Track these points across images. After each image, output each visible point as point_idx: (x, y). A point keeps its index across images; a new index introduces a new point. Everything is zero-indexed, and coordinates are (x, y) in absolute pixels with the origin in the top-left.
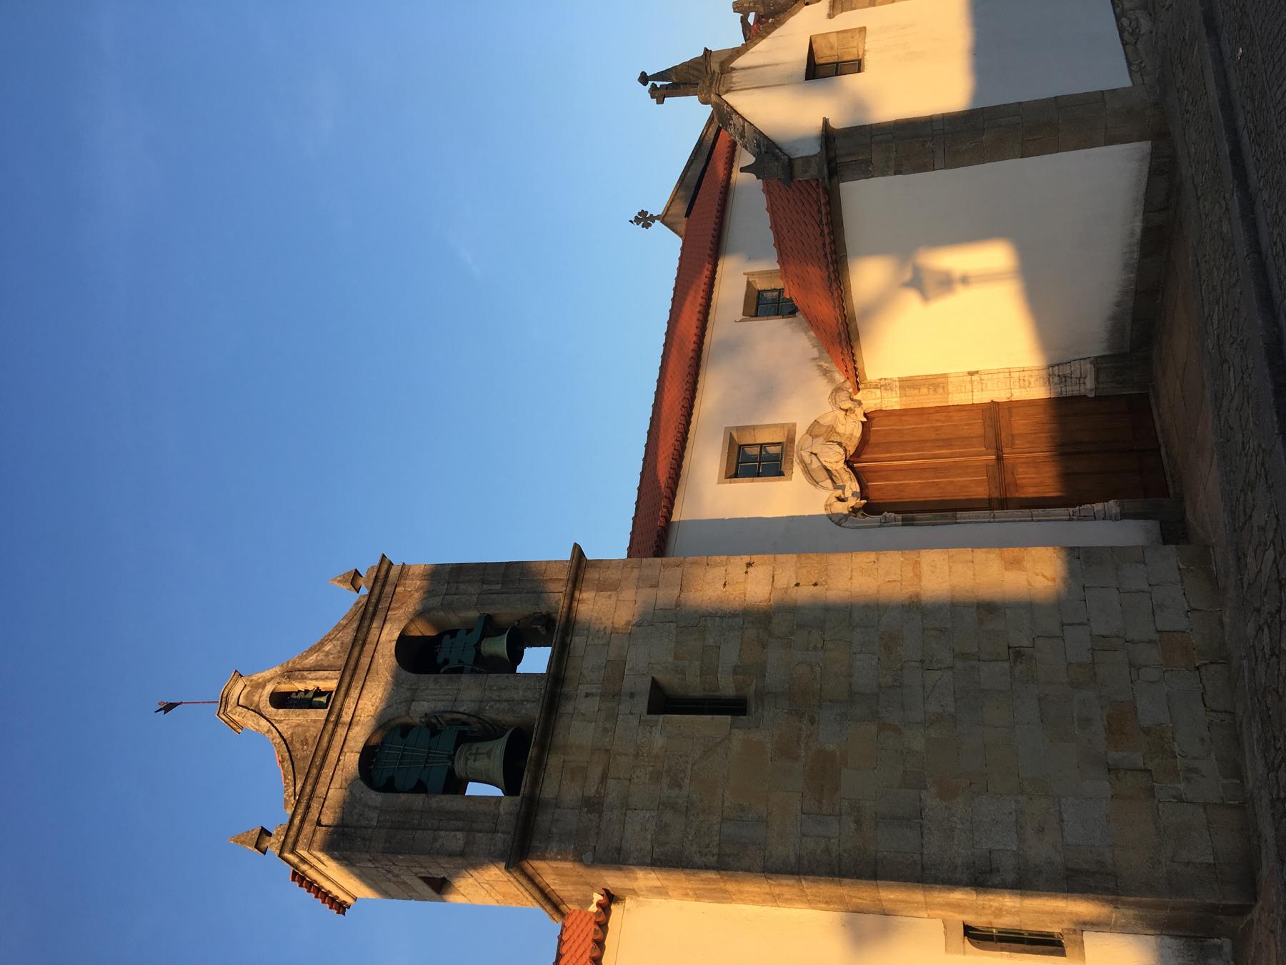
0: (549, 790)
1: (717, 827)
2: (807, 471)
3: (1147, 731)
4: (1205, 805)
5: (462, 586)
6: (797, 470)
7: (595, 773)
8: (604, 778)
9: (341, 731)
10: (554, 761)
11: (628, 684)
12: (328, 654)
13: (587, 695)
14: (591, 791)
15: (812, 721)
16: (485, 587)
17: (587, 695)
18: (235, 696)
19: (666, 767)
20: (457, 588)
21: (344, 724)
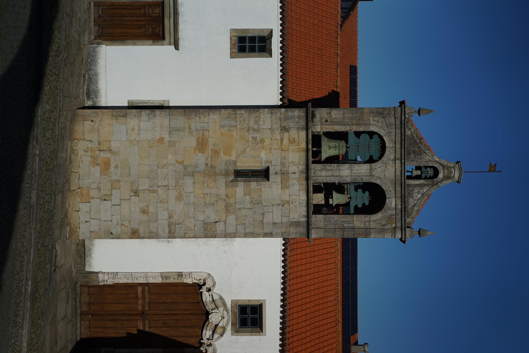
0: (303, 134)
1: (238, 124)
2: (225, 305)
3: (98, 164)
4: (84, 140)
5: (363, 226)
6: (229, 306)
7: (286, 142)
8: (282, 139)
9: (398, 156)
10: (303, 145)
11: (278, 178)
12: (419, 192)
13: (295, 173)
14: (286, 135)
15: (207, 164)
16: (352, 225)
17: (295, 173)
18: (456, 172)
19: (259, 145)
20: (365, 225)
21: (398, 159)
